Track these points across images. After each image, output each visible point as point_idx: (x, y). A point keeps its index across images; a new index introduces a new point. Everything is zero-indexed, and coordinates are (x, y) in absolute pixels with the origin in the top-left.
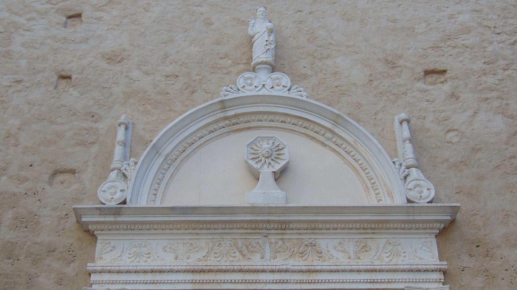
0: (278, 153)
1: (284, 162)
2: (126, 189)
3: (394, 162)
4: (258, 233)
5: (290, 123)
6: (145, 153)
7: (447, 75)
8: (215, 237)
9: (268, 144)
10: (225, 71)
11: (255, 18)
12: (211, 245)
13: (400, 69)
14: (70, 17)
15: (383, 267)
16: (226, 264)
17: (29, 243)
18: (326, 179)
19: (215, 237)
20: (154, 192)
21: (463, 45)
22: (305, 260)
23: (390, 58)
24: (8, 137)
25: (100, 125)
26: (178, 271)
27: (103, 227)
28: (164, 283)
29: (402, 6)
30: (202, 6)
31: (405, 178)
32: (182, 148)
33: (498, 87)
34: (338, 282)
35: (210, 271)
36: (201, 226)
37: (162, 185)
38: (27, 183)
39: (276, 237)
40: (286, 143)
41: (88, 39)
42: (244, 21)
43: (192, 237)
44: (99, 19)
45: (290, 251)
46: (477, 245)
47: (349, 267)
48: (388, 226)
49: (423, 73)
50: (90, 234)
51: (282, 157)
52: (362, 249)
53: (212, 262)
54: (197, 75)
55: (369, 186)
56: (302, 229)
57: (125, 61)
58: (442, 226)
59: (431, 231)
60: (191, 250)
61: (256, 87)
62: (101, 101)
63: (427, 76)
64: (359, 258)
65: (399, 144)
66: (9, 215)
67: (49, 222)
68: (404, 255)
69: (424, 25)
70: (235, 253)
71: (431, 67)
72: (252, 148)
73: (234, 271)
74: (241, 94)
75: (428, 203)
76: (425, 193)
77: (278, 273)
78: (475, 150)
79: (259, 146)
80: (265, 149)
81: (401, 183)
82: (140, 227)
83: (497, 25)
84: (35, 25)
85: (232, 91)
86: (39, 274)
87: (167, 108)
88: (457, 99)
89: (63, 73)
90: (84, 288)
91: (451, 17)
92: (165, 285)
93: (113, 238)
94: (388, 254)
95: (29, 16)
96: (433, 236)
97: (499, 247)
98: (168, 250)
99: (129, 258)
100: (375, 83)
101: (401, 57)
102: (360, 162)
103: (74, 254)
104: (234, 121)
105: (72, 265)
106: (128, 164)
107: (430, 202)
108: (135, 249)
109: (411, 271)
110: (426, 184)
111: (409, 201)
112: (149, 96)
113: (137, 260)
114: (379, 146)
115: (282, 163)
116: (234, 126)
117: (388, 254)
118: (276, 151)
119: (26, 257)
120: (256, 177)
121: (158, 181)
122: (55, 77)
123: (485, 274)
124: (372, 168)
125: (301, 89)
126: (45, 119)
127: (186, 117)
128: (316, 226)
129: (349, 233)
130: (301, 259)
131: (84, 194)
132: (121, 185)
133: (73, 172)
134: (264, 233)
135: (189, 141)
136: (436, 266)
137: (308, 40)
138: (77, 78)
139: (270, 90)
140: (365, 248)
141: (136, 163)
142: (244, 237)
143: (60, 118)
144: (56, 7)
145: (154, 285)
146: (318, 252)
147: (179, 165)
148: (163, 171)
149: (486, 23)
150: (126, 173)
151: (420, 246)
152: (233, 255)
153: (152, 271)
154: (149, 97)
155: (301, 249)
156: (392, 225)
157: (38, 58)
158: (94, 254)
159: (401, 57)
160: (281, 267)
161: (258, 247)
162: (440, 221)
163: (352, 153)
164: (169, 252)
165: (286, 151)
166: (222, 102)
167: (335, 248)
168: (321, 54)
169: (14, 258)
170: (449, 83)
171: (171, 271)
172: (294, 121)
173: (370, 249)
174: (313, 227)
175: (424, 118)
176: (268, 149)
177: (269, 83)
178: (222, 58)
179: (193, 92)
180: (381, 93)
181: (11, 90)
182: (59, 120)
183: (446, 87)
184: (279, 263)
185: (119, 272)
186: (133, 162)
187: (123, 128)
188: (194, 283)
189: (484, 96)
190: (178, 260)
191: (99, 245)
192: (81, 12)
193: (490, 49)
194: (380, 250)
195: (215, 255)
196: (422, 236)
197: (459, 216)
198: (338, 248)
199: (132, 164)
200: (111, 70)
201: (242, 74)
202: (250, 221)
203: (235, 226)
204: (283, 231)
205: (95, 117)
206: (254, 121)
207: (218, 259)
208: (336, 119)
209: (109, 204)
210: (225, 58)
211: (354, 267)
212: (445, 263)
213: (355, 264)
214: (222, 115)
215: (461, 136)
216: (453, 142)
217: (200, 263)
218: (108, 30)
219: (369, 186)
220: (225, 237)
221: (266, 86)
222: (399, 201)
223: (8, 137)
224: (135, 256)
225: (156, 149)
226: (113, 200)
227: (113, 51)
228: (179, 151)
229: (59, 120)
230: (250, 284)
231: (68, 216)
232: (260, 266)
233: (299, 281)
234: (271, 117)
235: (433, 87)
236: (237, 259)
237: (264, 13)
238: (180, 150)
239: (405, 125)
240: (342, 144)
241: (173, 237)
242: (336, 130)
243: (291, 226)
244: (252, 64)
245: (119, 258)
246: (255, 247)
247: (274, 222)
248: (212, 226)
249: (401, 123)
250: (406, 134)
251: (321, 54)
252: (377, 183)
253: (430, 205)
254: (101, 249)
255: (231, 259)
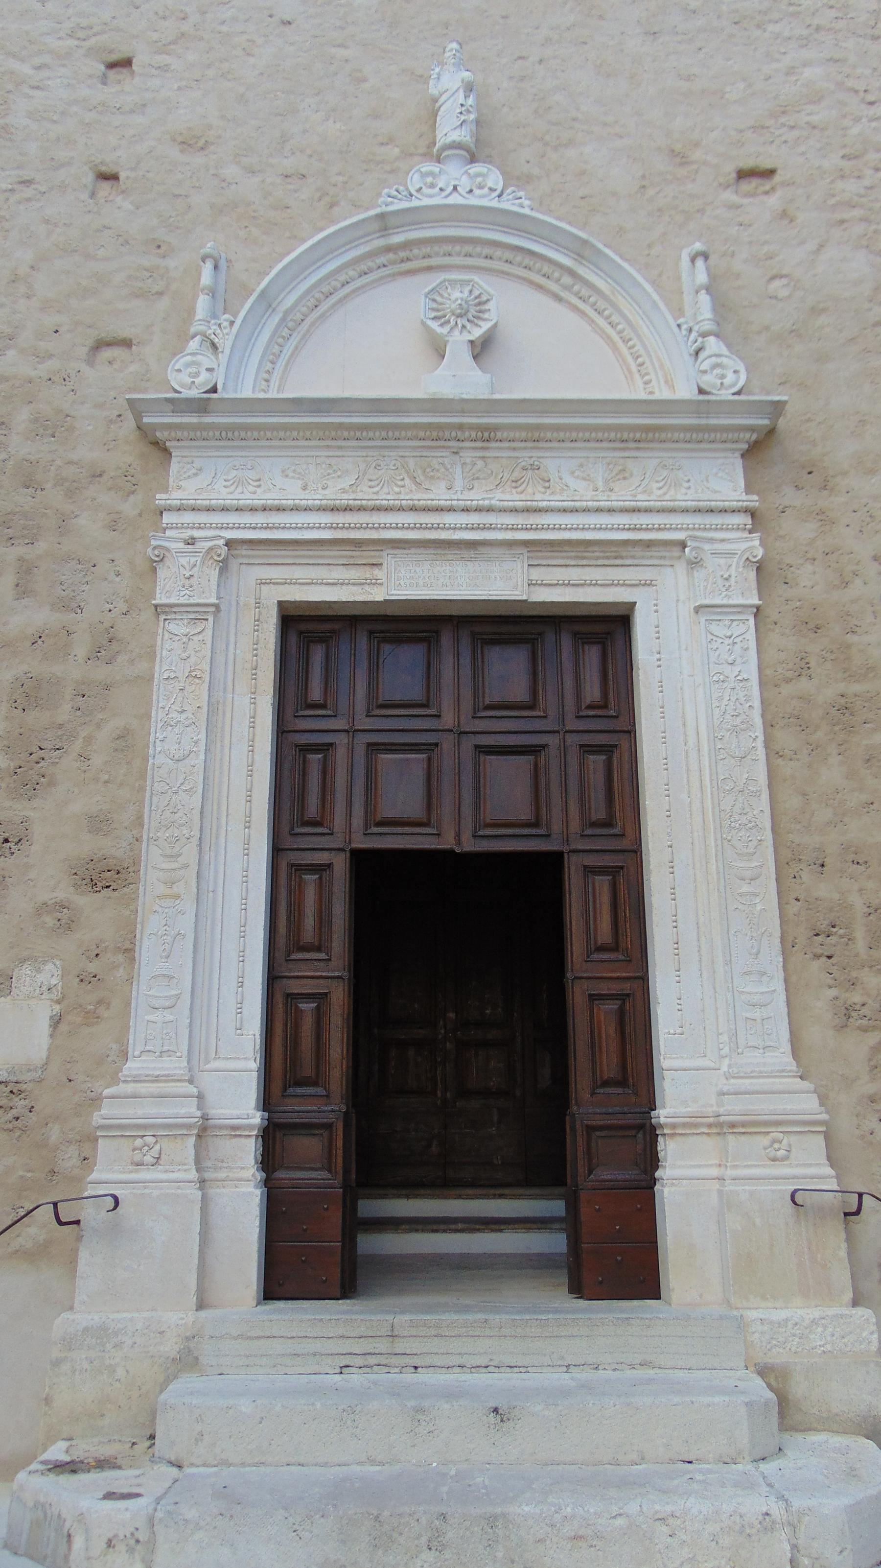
0: (478, 308)
1: (489, 325)
2: (215, 367)
3: (679, 326)
4: (444, 447)
5: (500, 259)
6: (247, 306)
7: (777, 179)
8: (370, 454)
9: (461, 292)
10: (388, 168)
11: (442, 64)
12: (363, 466)
13: (695, 167)
14: (112, 66)
15: (652, 503)
16: (389, 497)
17: (58, 462)
18: (557, 355)
19: (370, 454)
20: (266, 376)
21: (807, 123)
22: (521, 493)
23: (678, 147)
24: (14, 281)
25: (171, 263)
26: (308, 509)
27: (179, 434)
28: (284, 528)
29: (703, 50)
30: (346, 47)
31: (697, 353)
32: (313, 302)
33: (864, 200)
34: (576, 529)
35: (361, 509)
36: (346, 434)
37: (278, 364)
38: (50, 362)
39: (472, 455)
40: (492, 292)
41: (144, 105)
42: (421, 76)
43: (331, 454)
44: (164, 68)
45: (496, 477)
46: (809, 470)
47: (595, 503)
48: (663, 436)
49: (734, 175)
50: (158, 448)
51: (486, 316)
52: (617, 474)
53: (365, 494)
54: (339, 174)
55: (634, 368)
56: (518, 441)
57: (212, 147)
58: (754, 437)
59: (734, 446)
60: (329, 474)
61: (441, 189)
62: (172, 219)
63: (742, 181)
64: (611, 490)
65: (687, 298)
66: (22, 417)
67: (90, 428)
68: (686, 485)
69: (741, 86)
70: (403, 480)
71: (748, 163)
72: (434, 300)
73: (401, 509)
74: (415, 203)
75: (734, 394)
76: (730, 378)
77: (477, 513)
78: (816, 311)
79: (446, 295)
80: (457, 300)
81: (690, 361)
82: (243, 434)
83: (869, 88)
84: (49, 78)
85: (400, 196)
86: (78, 513)
87: (287, 234)
88: (791, 221)
89: (103, 169)
90: (152, 534)
91: (790, 71)
92: (286, 531)
93: (199, 454)
94: (661, 484)
95: (37, 61)
96: (738, 454)
97: (845, 473)
98: (291, 474)
99: (225, 487)
100: (651, 192)
101: (697, 145)
102: (620, 327)
103: (134, 481)
104: (402, 254)
105: (132, 498)
106: (220, 325)
107: (738, 393)
108: (234, 473)
109: (698, 511)
110: (732, 363)
111: (701, 391)
112: (254, 211)
113: (240, 490)
114: (656, 297)
115: (486, 326)
116: (403, 265)
117: (661, 484)
118: (476, 305)
119: (55, 485)
120: (439, 350)
121: (271, 357)
122: (90, 177)
123: (819, 517)
124: (639, 337)
125: (521, 194)
126: (76, 251)
127: (319, 242)
128: (542, 435)
129: (596, 449)
130: (514, 491)
131: (148, 381)
132: (207, 360)
133: (127, 343)
134: (453, 447)
135: (326, 289)
136: (741, 503)
137: (536, 111)
138: (128, 178)
139: (467, 196)
140: (623, 474)
141: (232, 323)
142: (418, 454)
143: (103, 249)
144: (87, 44)
145: (268, 531)
146: (543, 480)
147: (308, 331)
148: (280, 340)
149: (850, 83)
150: (216, 340)
151: (715, 470)
152: (400, 483)
153: (264, 509)
154: (255, 214)
155: (516, 475)
156: (669, 435)
157: (58, 139)
158: (168, 481)
159: (697, 145)
160: (481, 502)
161: (443, 470)
162: (752, 429)
163: (606, 313)
164: (293, 478)
165: (491, 305)
166: (382, 216)
167: (573, 473)
168: (558, 138)
169: (36, 486)
170: (779, 193)
171: (295, 509)
172: (508, 255)
173: (631, 475)
174: (536, 437)
175: (733, 255)
176: (462, 299)
177: (465, 183)
178: (382, 144)
179: (332, 206)
180: (659, 210)
181: (14, 198)
182: (101, 253)
183: (773, 201)
184: (477, 496)
185: (209, 509)
186: (226, 320)
187: (209, 265)
188: (335, 528)
189: (838, 216)
190: (307, 492)
191: (175, 466)
192: (130, 55)
193: (855, 130)
194: (647, 476)
195: (370, 483)
196: (717, 455)
197: (781, 423)
198: (577, 473)
199: (226, 324)
200: (188, 164)
201: (417, 167)
202: (430, 426)
203: (403, 433)
204: (485, 444)
205: (163, 248)
206: (437, 254)
207: (375, 490)
208: (582, 250)
209: (187, 393)
210: (387, 144)
211: (602, 504)
212: (755, 497)
213: (605, 498)
214: (381, 242)
215: (795, 286)
216: (780, 296)
217: (345, 496)
218: (179, 89)
219: (634, 368)
220: (386, 453)
221: (458, 188)
222: (685, 392)
223: (14, 281)
224: (235, 484)
225: (266, 300)
226: (194, 387)
227: (189, 129)
228: (308, 307)
229: (101, 253)
230: (428, 531)
231: (122, 418)
232: (446, 500)
233: (510, 526)
234: (468, 248)
235: (751, 200)
236: (407, 490)
237: (458, 54)
238: (309, 304)
239: (700, 263)
240: (590, 297)
241: (299, 454)
242: (581, 271)
243: (499, 435)
244: (435, 150)
245: (210, 487)
246: (438, 471)
247: (471, 427)
248: (365, 434)
249: (693, 260)
250: (702, 278)
251: (558, 138)
252: (648, 364)
253: (736, 397)
254: (179, 472)
255: (397, 489)
